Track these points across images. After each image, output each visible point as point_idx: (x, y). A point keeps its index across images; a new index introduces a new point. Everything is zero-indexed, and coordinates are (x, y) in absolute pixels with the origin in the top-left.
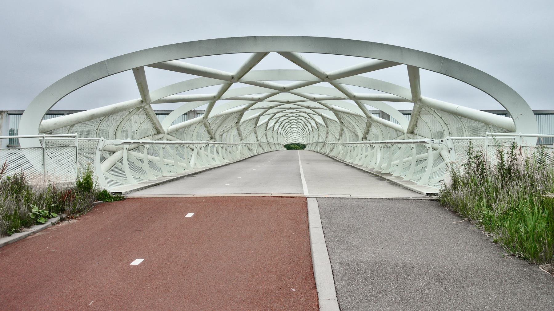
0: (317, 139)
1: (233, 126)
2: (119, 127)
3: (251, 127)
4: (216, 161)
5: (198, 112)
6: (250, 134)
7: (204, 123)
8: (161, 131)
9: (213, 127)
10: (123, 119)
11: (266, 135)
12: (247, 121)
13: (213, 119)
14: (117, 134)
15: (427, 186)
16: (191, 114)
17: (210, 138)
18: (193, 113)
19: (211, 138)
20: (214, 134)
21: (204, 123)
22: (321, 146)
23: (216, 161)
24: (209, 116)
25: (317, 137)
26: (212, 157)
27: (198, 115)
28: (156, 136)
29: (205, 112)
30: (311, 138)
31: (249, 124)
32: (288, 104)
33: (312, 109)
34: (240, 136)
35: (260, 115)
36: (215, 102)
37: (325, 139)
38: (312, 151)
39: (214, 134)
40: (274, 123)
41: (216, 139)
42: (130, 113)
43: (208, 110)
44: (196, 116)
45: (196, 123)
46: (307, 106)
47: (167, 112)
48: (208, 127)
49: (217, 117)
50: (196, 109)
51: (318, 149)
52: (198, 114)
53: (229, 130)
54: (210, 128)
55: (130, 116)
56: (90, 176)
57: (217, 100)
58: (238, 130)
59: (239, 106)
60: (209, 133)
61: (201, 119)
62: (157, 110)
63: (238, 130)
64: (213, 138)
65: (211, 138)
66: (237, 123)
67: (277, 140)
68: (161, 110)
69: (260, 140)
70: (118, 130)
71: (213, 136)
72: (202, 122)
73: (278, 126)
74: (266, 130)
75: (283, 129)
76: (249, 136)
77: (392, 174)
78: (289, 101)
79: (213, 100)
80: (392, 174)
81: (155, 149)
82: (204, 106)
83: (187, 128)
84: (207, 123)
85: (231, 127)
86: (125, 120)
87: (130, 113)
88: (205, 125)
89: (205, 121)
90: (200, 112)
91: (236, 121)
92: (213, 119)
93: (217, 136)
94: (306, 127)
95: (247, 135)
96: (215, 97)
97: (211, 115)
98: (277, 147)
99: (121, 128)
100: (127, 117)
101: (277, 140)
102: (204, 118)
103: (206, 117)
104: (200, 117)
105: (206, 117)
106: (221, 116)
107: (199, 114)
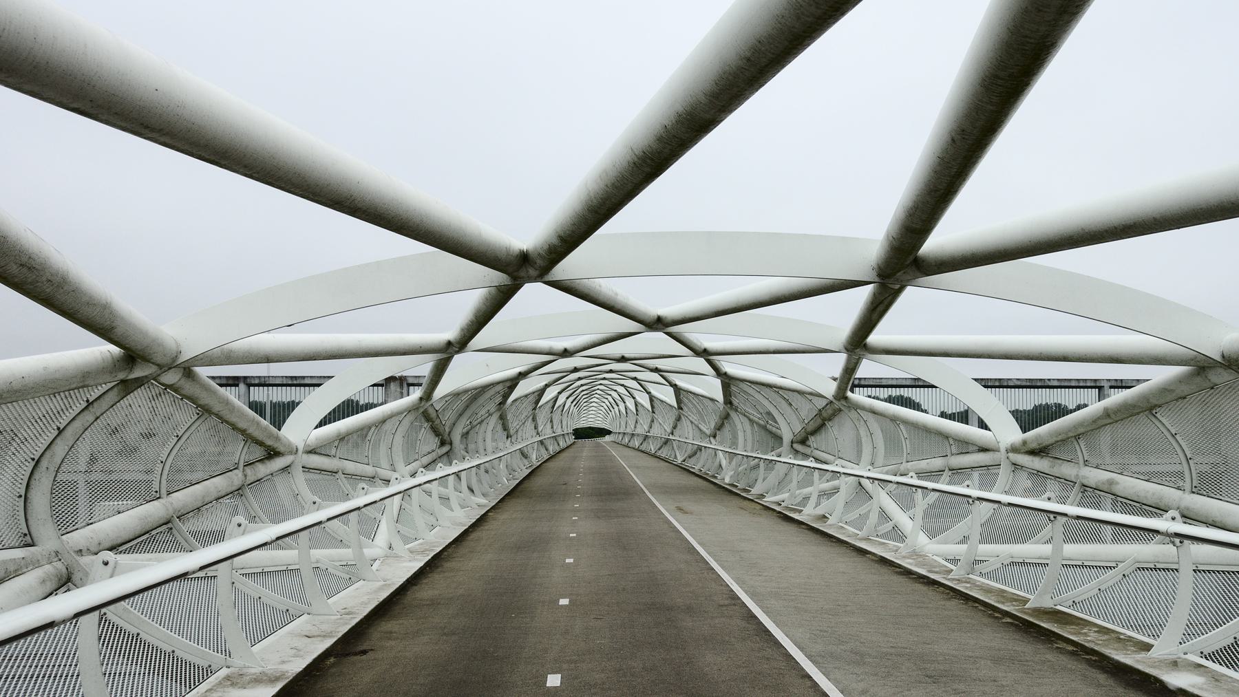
0: (633, 427)
1: (493, 410)
2: (44, 463)
3: (527, 407)
4: (452, 510)
5: (411, 381)
6: (523, 424)
7: (425, 413)
8: (281, 449)
9: (447, 418)
10: (60, 431)
11: (551, 421)
12: (520, 398)
13: (447, 399)
14: (32, 494)
15: (874, 538)
16: (393, 387)
17: (439, 443)
18: (398, 382)
19: (443, 443)
20: (450, 432)
21: (422, 410)
22: (641, 439)
23: (452, 510)
24: (470, 343)
25: (634, 425)
26: (439, 495)
27: (411, 388)
28: (260, 467)
29: (425, 382)
30: (623, 424)
31: (525, 404)
32: (566, 357)
33: (661, 373)
34: (505, 430)
35: (546, 385)
36: (448, 360)
37: (647, 430)
38: (624, 445)
39: (450, 432)
40: (558, 391)
41: (453, 445)
42: (90, 404)
43: (432, 380)
44: (405, 391)
45: (399, 413)
46: (655, 367)
47: (314, 381)
48: (434, 420)
49: (456, 395)
50: (404, 374)
51: (636, 443)
52: (409, 385)
53: (482, 421)
54: (437, 422)
55: (88, 417)
56: (283, 455)
57: (458, 352)
58: (502, 418)
59: (507, 367)
60: (436, 431)
61: (413, 402)
62: (311, 377)
63: (502, 418)
64: (447, 442)
65: (443, 443)
66: (500, 404)
67: (562, 427)
68: (321, 377)
69: (541, 431)
70: (36, 476)
71: (446, 437)
72: (417, 408)
73: (565, 398)
74: (552, 412)
75: (574, 403)
76: (522, 428)
77: (802, 511)
78: (626, 355)
79: (447, 352)
80: (802, 511)
81: (252, 512)
82: (422, 367)
83: (373, 429)
84: (431, 411)
85: (487, 414)
86: (69, 433)
87: (90, 404)
88: (427, 417)
89: (426, 407)
90: (415, 381)
91: (499, 399)
92: (447, 399)
93: (456, 437)
94: (615, 406)
95: (518, 427)
96: (449, 343)
97: (443, 389)
98: (567, 440)
99: (52, 469)
100: (77, 424)
101: (562, 427)
102: (421, 399)
103: (427, 396)
104: (416, 393)
105: (427, 396)
106: (466, 391)
107: (413, 385)
